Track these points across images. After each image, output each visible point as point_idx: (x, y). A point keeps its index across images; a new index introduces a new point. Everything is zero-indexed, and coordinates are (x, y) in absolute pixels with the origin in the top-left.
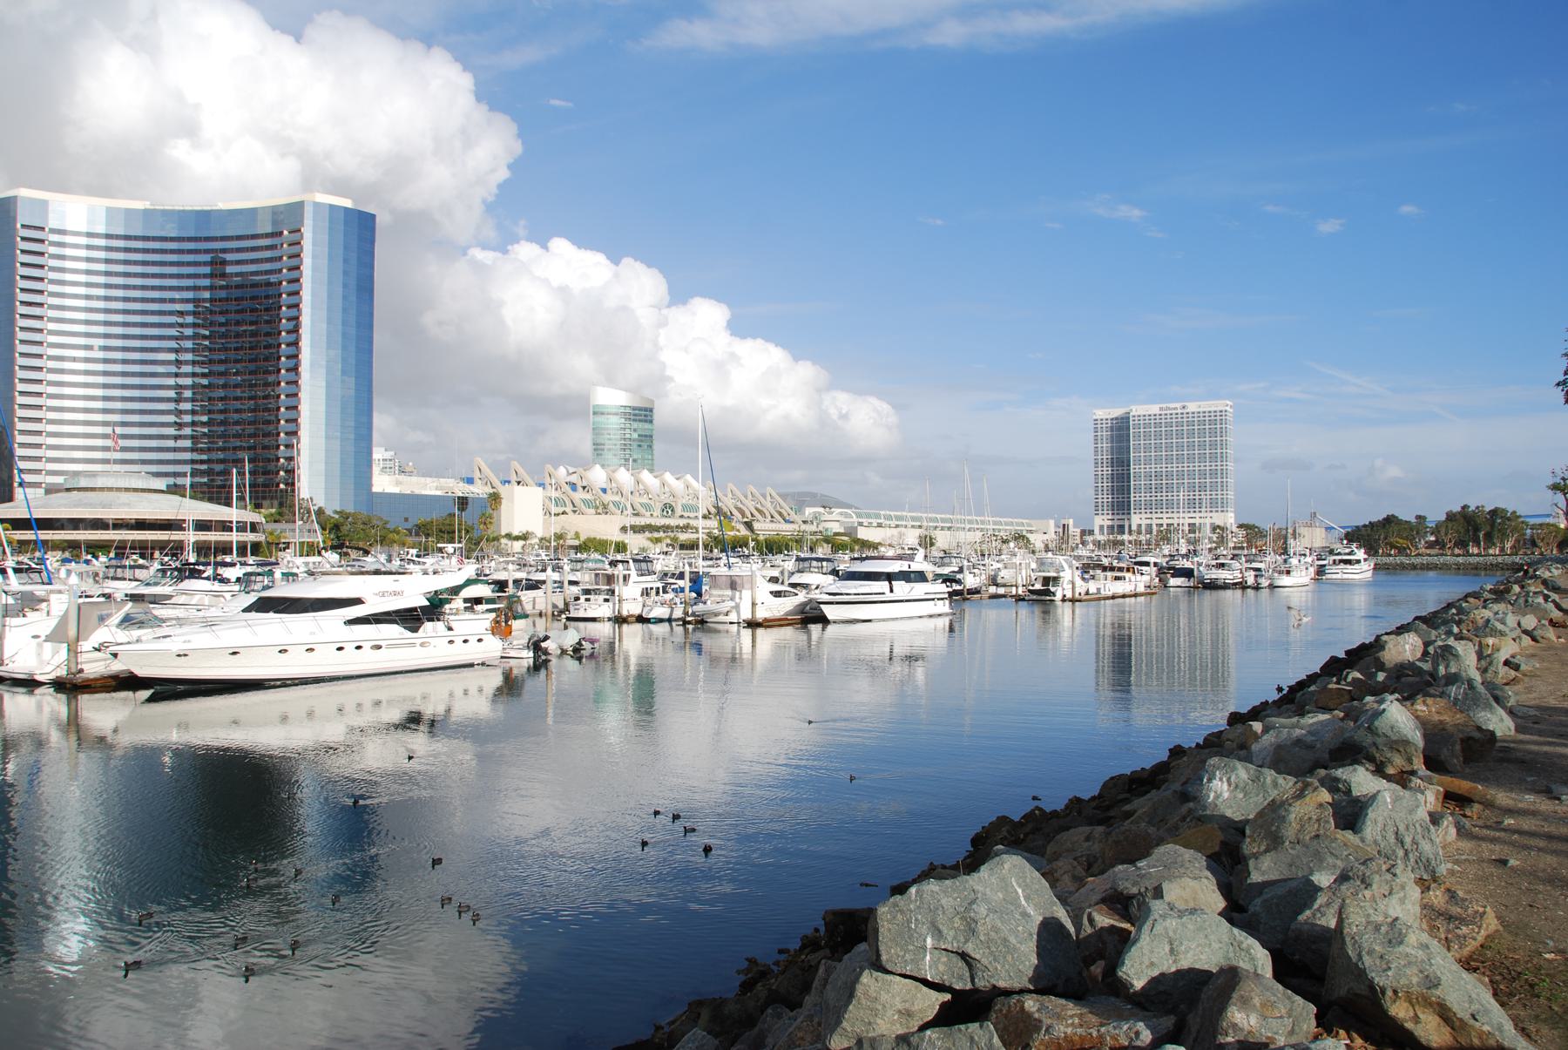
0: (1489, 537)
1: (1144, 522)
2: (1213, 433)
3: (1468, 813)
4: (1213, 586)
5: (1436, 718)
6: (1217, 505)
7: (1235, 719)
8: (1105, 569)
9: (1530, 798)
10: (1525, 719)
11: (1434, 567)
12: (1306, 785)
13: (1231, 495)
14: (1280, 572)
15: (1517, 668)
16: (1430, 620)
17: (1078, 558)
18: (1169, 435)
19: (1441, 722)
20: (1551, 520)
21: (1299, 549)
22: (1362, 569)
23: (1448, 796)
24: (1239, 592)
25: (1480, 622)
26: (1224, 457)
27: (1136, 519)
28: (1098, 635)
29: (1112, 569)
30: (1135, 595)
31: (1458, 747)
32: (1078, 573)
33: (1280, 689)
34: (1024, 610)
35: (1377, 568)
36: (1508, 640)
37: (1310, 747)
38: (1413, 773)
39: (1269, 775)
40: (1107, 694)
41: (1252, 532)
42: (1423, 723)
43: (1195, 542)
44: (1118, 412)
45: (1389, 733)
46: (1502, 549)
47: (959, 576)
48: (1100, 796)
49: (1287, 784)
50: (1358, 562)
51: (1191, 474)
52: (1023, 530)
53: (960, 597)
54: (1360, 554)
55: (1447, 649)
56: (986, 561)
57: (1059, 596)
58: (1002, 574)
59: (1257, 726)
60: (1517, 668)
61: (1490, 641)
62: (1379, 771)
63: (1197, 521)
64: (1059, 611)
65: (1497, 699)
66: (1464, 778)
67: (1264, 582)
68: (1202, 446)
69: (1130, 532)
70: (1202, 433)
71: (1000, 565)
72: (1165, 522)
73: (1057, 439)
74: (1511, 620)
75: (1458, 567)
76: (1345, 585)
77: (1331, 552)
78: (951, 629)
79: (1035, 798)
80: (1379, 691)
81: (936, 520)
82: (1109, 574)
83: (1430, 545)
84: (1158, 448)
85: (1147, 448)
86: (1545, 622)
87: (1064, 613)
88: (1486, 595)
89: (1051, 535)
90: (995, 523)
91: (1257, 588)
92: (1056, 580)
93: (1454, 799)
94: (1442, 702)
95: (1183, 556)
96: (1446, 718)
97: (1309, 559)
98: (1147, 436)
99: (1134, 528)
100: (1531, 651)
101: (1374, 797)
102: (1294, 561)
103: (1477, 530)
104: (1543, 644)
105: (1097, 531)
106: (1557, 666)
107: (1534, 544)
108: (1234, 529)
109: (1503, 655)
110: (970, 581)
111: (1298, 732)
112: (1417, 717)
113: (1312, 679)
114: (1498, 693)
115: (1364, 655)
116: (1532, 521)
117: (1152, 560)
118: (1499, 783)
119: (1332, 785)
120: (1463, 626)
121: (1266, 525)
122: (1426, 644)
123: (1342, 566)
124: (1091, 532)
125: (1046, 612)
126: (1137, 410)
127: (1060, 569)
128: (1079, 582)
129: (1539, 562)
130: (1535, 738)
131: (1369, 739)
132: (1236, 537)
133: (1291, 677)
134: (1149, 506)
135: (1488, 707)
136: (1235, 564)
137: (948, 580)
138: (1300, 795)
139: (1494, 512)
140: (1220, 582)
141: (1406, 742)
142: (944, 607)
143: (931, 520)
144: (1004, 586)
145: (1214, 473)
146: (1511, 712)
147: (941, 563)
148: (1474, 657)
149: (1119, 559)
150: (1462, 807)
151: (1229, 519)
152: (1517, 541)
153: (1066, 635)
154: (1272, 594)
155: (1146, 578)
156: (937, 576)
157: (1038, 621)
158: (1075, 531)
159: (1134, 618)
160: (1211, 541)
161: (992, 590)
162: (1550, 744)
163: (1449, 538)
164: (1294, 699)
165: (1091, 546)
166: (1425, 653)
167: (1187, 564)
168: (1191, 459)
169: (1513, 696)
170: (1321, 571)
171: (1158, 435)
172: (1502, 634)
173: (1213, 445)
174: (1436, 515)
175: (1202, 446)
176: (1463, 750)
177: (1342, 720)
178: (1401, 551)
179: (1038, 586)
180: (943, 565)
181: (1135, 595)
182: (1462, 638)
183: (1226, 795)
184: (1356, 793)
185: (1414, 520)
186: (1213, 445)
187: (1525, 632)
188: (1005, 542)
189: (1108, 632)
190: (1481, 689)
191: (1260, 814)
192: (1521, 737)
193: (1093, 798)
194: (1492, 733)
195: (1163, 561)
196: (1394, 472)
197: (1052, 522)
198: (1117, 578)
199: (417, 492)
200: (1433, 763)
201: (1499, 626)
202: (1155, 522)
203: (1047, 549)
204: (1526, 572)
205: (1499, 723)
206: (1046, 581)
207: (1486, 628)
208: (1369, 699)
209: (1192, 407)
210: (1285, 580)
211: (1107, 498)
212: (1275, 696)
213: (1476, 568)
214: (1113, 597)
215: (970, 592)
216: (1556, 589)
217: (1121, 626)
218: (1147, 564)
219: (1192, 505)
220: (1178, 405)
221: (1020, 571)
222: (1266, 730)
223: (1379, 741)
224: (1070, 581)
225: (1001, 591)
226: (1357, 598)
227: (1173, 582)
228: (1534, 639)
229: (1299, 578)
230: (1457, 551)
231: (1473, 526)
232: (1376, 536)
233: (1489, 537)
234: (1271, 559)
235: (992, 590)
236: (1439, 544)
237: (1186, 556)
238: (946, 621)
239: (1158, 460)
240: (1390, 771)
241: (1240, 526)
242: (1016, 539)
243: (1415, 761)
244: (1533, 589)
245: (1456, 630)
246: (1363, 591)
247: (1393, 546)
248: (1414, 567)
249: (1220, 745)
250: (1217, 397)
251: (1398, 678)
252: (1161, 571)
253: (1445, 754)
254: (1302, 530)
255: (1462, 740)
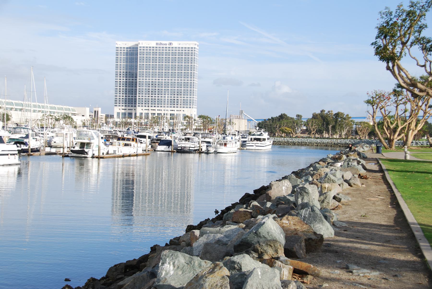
0: (334, 128)
1: (144, 112)
2: (186, 60)
3: (305, 280)
4: (182, 151)
5: (293, 227)
6: (187, 104)
7: (190, 228)
8: (119, 139)
9: (338, 271)
10: (341, 229)
11: (305, 144)
12: (216, 266)
13: (195, 98)
14: (221, 144)
15: (339, 200)
16: (298, 174)
17: (103, 132)
18: (161, 60)
19: (295, 230)
20: (365, 120)
21: (233, 131)
22: (267, 144)
23: (296, 271)
24: (197, 155)
25: (323, 175)
26: (192, 76)
27: (139, 110)
28: (114, 180)
29: (123, 139)
30: (137, 155)
31: (303, 244)
32: (103, 140)
33: (217, 212)
34: (67, 162)
35: (274, 143)
36: (336, 185)
37: (225, 244)
38: (278, 258)
39: (197, 260)
40: (118, 216)
41: (205, 120)
42: (285, 230)
43: (174, 125)
44: (131, 44)
45: (267, 236)
46: (340, 136)
47: (26, 140)
48: (107, 276)
49: (207, 265)
50: (264, 140)
51: (173, 85)
52: (70, 113)
53: (26, 153)
54: (266, 135)
55: (303, 189)
56: (44, 132)
57: (90, 155)
58: (54, 140)
59: (197, 232)
60: (339, 200)
61: (327, 185)
62: (260, 258)
63: (175, 113)
64: (90, 164)
65: (326, 217)
66: (305, 261)
67: (212, 150)
68: (180, 68)
69: (136, 117)
70: (180, 60)
71: (54, 134)
72: (157, 112)
73: (95, 60)
74: (339, 174)
75: (317, 145)
76: (257, 153)
77: (250, 134)
78: (19, 173)
79: (67, 280)
80: (265, 213)
81: (12, 104)
82: (122, 142)
83: (303, 132)
84: (154, 67)
85: (148, 67)
86: (356, 176)
87: (93, 164)
88: (329, 160)
89: (87, 117)
90: (51, 108)
91: (207, 153)
92: (88, 144)
93: (299, 273)
94: (296, 219)
95: (166, 133)
96: (298, 227)
97: (237, 137)
98: (148, 60)
99: (138, 115)
100: (348, 192)
101: (251, 273)
102: (229, 138)
103: (328, 124)
104: (354, 187)
105: (115, 116)
106: (360, 199)
107: (356, 133)
108: (197, 119)
109: (332, 194)
110: (33, 144)
111: (219, 236)
112: (283, 227)
113: (234, 206)
114: (327, 214)
115: (262, 192)
116: (356, 120)
117: (147, 135)
118: (323, 263)
119: (231, 266)
120: (314, 177)
121: (214, 117)
122: (294, 187)
123: (255, 142)
124: (112, 116)
125: (82, 164)
126: (143, 44)
127: (91, 138)
128: (102, 146)
129: (358, 143)
130: (344, 239)
131: (256, 239)
132: (198, 123)
133: (221, 207)
134: (147, 102)
135: (321, 221)
136: (196, 139)
137: (18, 142)
138: (212, 271)
139: (337, 115)
140: (186, 149)
141: (275, 241)
142: (15, 159)
143: (8, 104)
144: (56, 147)
145: (186, 85)
146: (334, 225)
147: (14, 131)
148: (317, 194)
149: (128, 133)
150: (302, 277)
151: (193, 112)
152: (348, 131)
153: (93, 180)
154: (216, 157)
155: (143, 145)
156: (11, 140)
157: (76, 170)
158: (102, 115)
159: (136, 170)
160: (183, 124)
161: (48, 150)
162: (351, 242)
163: (314, 128)
164: (222, 217)
165: (111, 125)
166: (293, 192)
167: (169, 138)
168: (173, 75)
169: (335, 216)
170: (243, 144)
171: (161, 60)
172: (333, 182)
173: (186, 68)
174: (307, 115)
175: (180, 68)
176: (306, 245)
177: (244, 229)
178: (288, 134)
179: (77, 148)
180: (15, 133)
181: (137, 155)
182: (312, 184)
183: (172, 273)
184: (244, 270)
185: (295, 117)
186: (186, 68)
187: (346, 181)
188: (57, 120)
189: (120, 178)
190: (318, 212)
191: (190, 284)
192: (338, 238)
193: (103, 278)
194: (322, 236)
195: (154, 136)
196: (286, 89)
197: (88, 109)
198: (126, 145)
199: (283, 252)
200: (290, 253)
201: (332, 177)
202: (150, 112)
203: (84, 125)
204: (351, 148)
205: (326, 231)
206: (83, 145)
207: (325, 178)
208: (260, 217)
209: (175, 44)
210: (222, 149)
211: (122, 96)
212: (214, 216)
213: (326, 146)
214: (123, 156)
215: (33, 150)
216: (365, 158)
217: (127, 174)
218: (144, 137)
219: (173, 103)
220: (167, 42)
221: (66, 138)
222: (201, 235)
223: (261, 240)
224: (97, 145)
225: (53, 150)
226: (262, 160)
227: (160, 148)
228: (350, 185)
229: (233, 146)
230: (317, 136)
231: (326, 122)
232: (276, 126)
233: (334, 128)
234: (217, 136)
235: (48, 150)
236: (308, 131)
237: (168, 133)
238: (16, 168)
239: (154, 75)
240: (266, 257)
241: (200, 117)
242: (64, 118)
243: (280, 251)
244: (352, 157)
245: (311, 179)
246: (266, 156)
247: (283, 132)
248: (294, 144)
249: (178, 244)
250: (189, 39)
251: (277, 205)
252: (153, 141)
253: (296, 248)
254: (235, 121)
255: (305, 240)
